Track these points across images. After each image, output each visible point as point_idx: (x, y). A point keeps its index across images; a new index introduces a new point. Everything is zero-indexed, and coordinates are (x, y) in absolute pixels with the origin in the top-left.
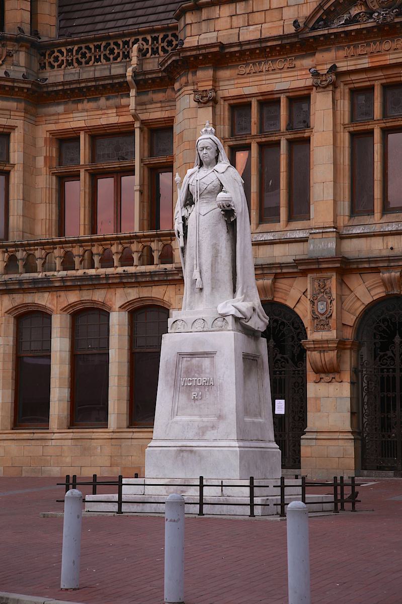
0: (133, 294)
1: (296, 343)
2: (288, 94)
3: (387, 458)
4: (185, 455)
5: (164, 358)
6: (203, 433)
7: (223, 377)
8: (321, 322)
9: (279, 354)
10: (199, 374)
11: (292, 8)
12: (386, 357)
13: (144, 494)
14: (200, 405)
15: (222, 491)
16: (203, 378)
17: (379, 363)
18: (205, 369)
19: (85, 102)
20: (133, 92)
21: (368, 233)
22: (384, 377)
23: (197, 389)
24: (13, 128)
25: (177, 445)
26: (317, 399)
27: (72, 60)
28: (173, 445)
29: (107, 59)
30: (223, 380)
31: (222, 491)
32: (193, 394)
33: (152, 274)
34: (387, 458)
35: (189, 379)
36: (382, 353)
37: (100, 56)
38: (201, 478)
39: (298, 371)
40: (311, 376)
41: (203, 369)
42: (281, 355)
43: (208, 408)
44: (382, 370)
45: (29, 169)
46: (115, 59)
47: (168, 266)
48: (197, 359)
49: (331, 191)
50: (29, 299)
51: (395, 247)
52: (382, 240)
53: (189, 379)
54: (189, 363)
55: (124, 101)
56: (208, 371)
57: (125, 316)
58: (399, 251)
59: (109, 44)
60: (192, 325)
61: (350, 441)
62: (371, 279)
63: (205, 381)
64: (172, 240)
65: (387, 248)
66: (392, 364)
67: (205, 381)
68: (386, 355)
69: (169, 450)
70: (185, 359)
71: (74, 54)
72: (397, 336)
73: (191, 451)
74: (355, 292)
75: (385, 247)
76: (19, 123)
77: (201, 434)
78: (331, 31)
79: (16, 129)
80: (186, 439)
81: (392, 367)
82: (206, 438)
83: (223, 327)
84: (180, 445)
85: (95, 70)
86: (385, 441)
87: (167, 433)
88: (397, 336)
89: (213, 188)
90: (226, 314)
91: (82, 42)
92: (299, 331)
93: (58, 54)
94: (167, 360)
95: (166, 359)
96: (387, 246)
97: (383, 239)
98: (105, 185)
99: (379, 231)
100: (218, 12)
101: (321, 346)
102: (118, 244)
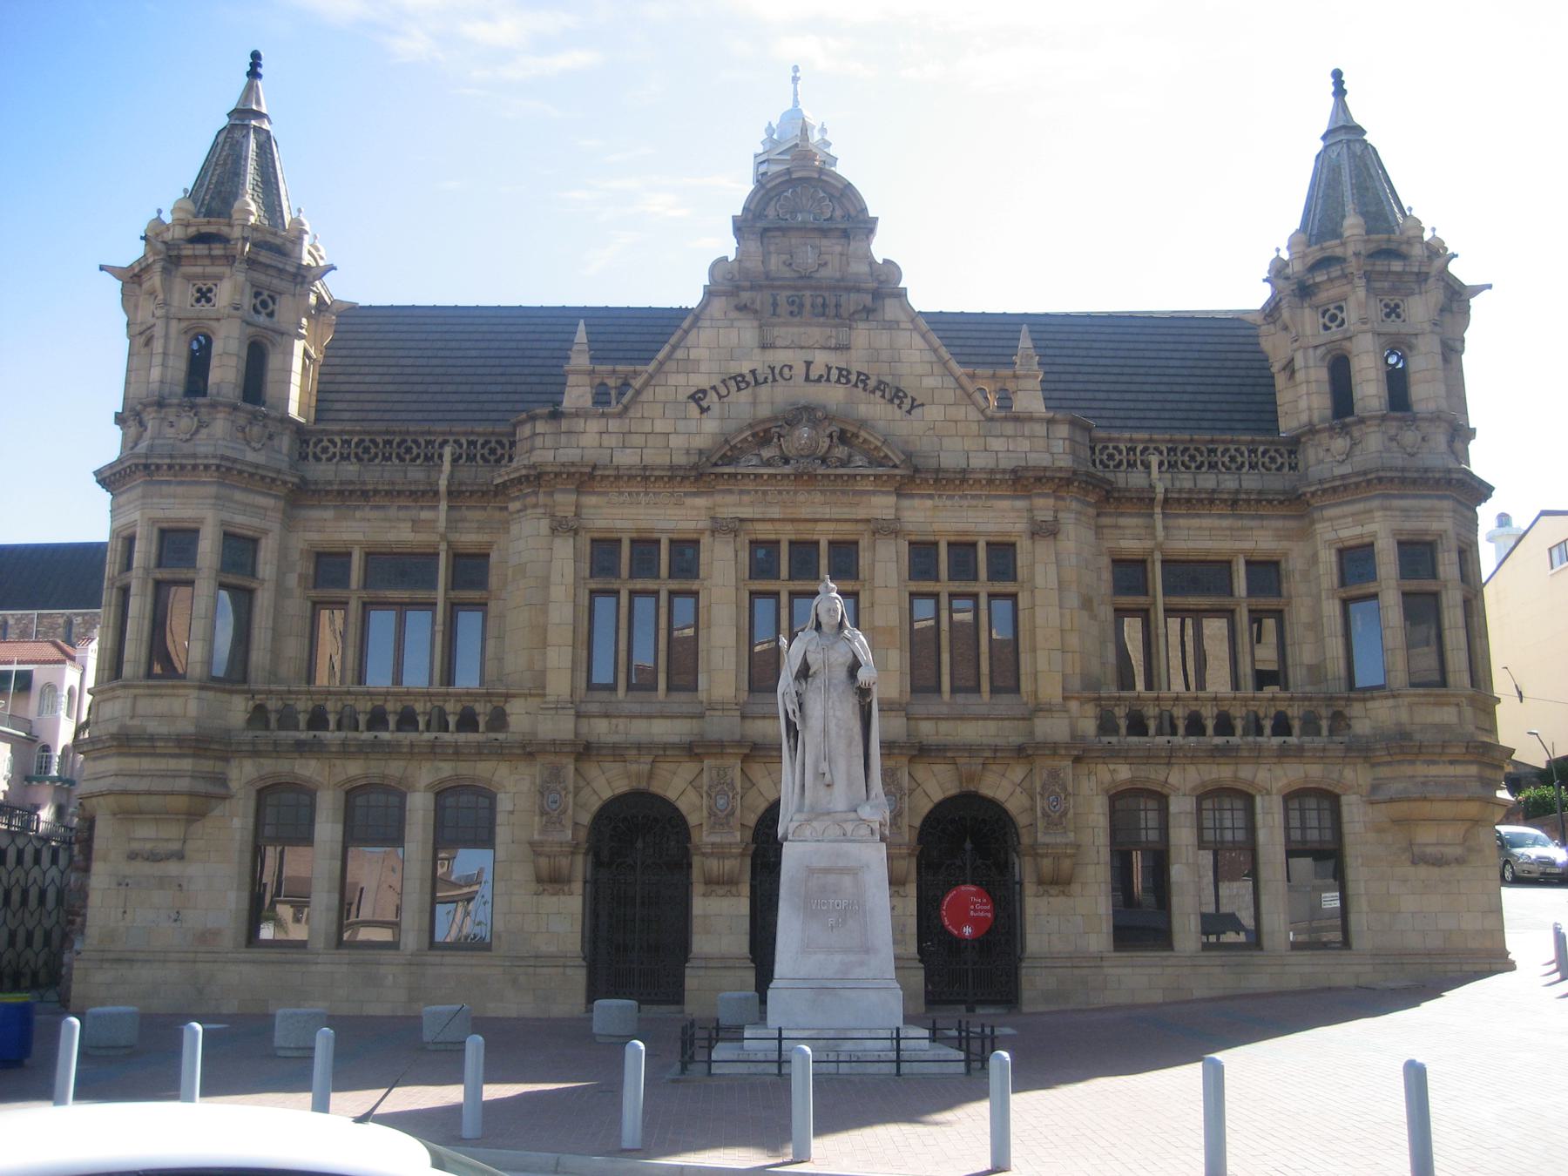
0: (446, 769)
2: (671, 536)
8: (719, 820)
11: (681, 437)
19: (367, 509)
20: (443, 505)
24: (266, 532)
26: (705, 916)
27: (349, 454)
29: (402, 459)
33: (479, 745)
36: (949, 862)
37: (391, 454)
38: (780, 1030)
40: (698, 889)
45: (281, 591)
46: (413, 460)
47: (501, 736)
49: (733, 659)
50: (466, 769)
55: (425, 515)
57: (430, 797)
59: (405, 441)
62: (614, 769)
64: (1346, 706)
68: (954, 864)
71: (1179, 454)
76: (276, 527)
78: (739, 471)
79: (270, 534)
85: (383, 471)
91: (1232, 442)
93: (329, 444)
98: (382, 622)
100: (583, 425)
101: (719, 852)
102: (486, 702)
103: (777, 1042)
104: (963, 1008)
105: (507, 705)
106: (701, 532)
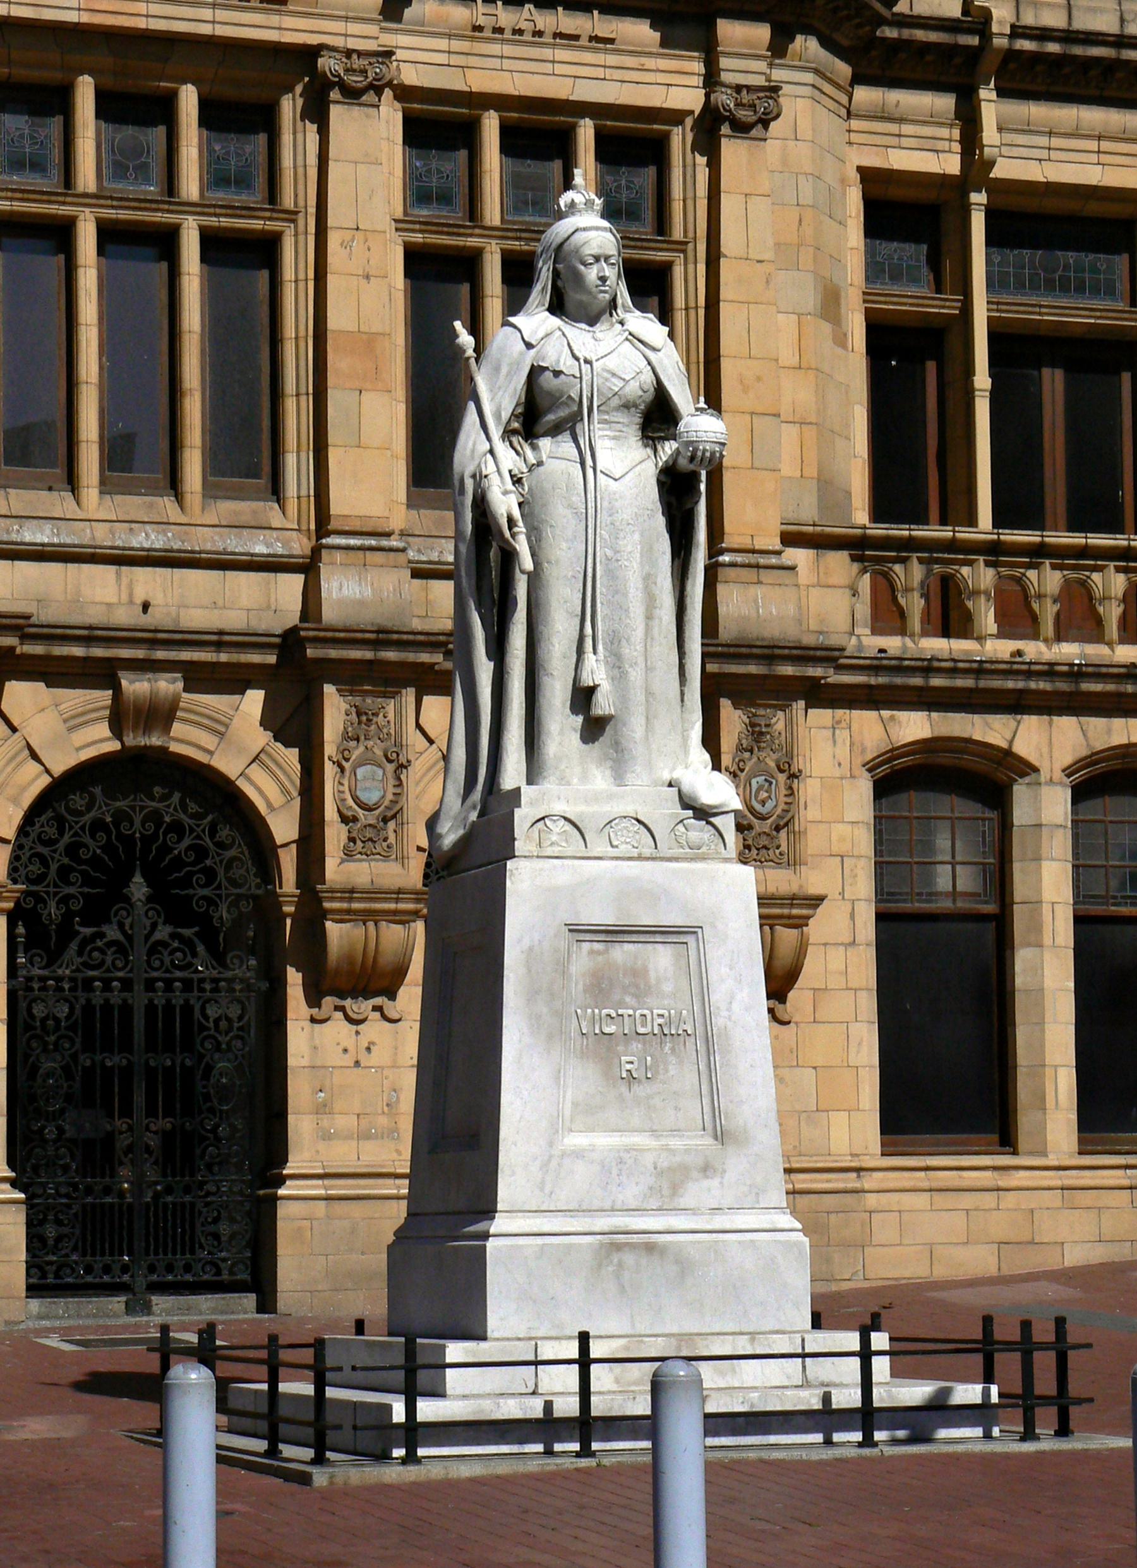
1: (224, 892)
3: (98, 1258)
4: (629, 1258)
5: (520, 941)
6: (675, 1189)
7: (729, 1009)
9: (164, 924)
10: (636, 996)
12: (99, 943)
13: (534, 1393)
14: (649, 1097)
15: (804, 1367)
16: (657, 1010)
17: (80, 960)
18: (659, 981)
21: (75, 546)
22: (174, 1006)
23: (636, 1046)
25: (597, 1229)
28: (580, 1229)
30: (730, 1018)
31: (804, 1367)
32: (629, 1059)
34: (98, 1258)
35: (605, 1012)
36: (87, 931)
38: (584, 1339)
39: (230, 981)
41: (653, 981)
42: (169, 929)
43: (676, 1108)
44: (88, 984)
48: (626, 946)
51: (157, 599)
52: (114, 576)
53: (605, 1012)
54: (600, 958)
56: (667, 987)
58: (168, 614)
60: (532, 826)
61: (13, 1208)
63: (661, 1021)
65: (131, 602)
66: (119, 964)
67: (661, 1021)
68: (102, 935)
69: (569, 1247)
70: (586, 946)
72: (138, 879)
73: (650, 1248)
74: (24, 732)
75: (125, 597)
77: (666, 1192)
80: (618, 1206)
81: (120, 974)
82: (683, 1202)
83: (704, 849)
84: (606, 1229)
86: (174, 1204)
87: (547, 1190)
88: (138, 879)
89: (641, 393)
90: (716, 807)
92: (41, 849)
94: (531, 949)
95: (526, 943)
96: (131, 595)
97: (118, 574)
99: (110, 544)
103: (856, 1362)
104: (117, 1303)
105: (995, 573)
106: (676, 117)
